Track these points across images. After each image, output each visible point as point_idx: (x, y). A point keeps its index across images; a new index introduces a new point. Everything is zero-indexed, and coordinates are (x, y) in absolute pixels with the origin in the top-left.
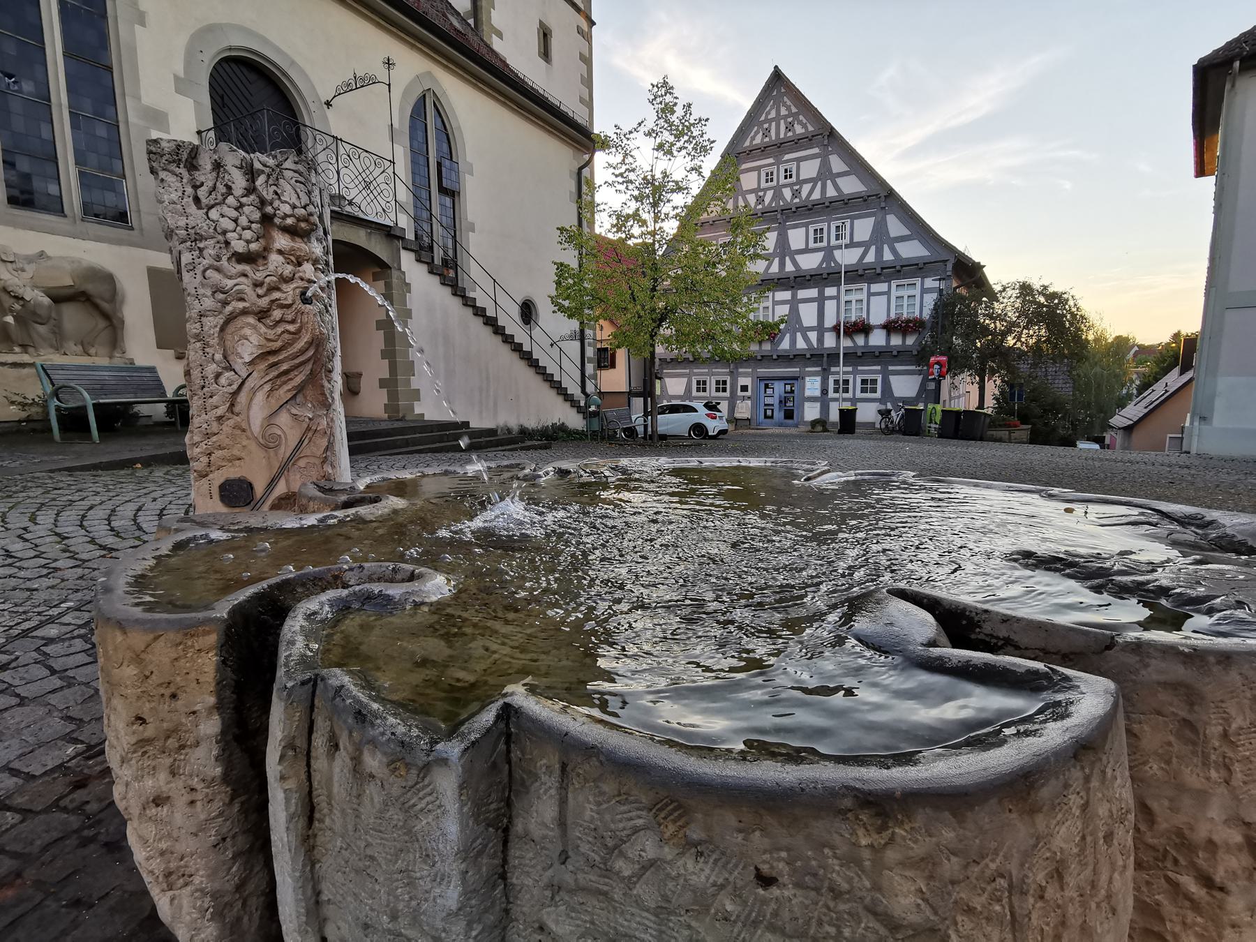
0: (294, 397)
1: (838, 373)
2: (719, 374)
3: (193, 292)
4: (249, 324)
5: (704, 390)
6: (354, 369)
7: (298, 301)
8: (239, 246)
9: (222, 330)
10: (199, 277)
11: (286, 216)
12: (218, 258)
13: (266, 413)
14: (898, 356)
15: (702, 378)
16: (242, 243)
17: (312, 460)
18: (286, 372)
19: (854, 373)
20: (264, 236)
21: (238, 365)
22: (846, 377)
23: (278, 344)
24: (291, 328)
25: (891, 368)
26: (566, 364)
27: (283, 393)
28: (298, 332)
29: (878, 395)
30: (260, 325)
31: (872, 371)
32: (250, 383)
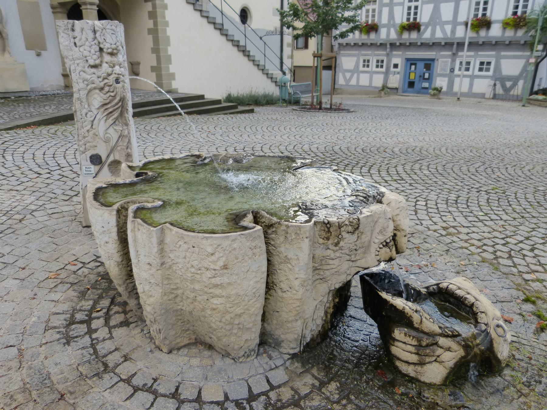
0: (115, 122)
1: (462, 56)
2: (379, 55)
3: (76, 81)
4: (96, 93)
5: (368, 66)
6: (134, 60)
7: (115, 83)
8: (91, 62)
9: (87, 95)
10: (78, 75)
11: (108, 48)
12: (84, 67)
13: (104, 129)
14: (510, 45)
15: (367, 58)
16: (92, 60)
17: (123, 147)
18: (111, 112)
19: (475, 57)
20: (101, 56)
21: (93, 109)
22: (468, 60)
23: (108, 101)
24: (112, 94)
25: (503, 53)
26: (268, 52)
27: (110, 121)
28: (114, 97)
29: (491, 73)
30: (101, 93)
31: (487, 55)
32: (98, 117)
